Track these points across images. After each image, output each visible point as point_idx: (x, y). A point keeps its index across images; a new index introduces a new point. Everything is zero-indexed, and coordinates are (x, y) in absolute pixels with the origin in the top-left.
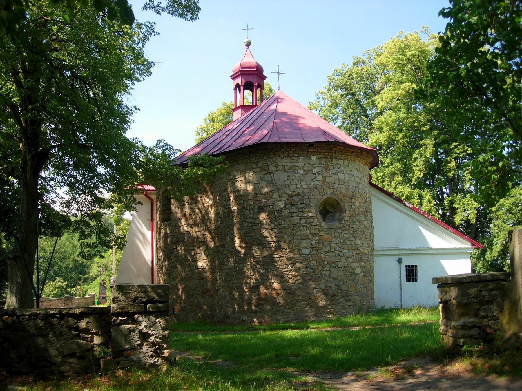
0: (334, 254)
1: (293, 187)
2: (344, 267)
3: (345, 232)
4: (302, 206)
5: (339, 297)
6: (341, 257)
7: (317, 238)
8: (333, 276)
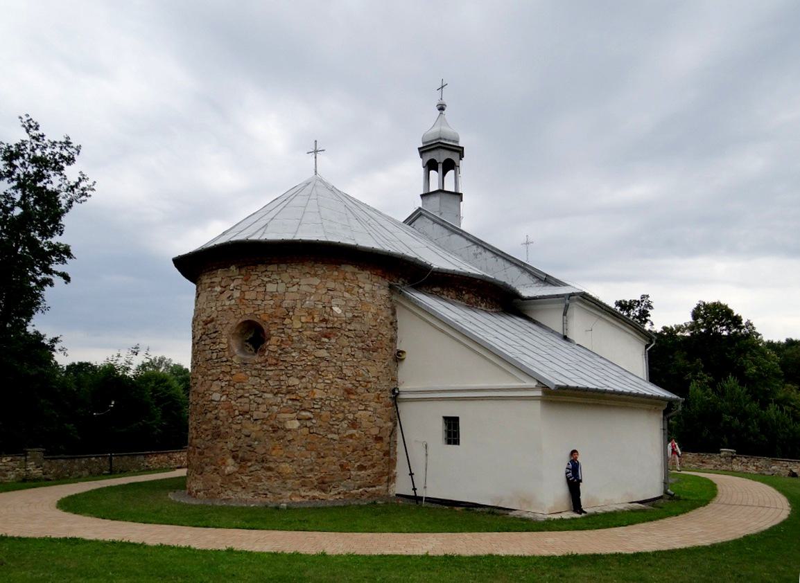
2: (263, 419)
3: (270, 368)
4: (214, 335)
5: (253, 463)
6: (258, 404)
7: (228, 378)
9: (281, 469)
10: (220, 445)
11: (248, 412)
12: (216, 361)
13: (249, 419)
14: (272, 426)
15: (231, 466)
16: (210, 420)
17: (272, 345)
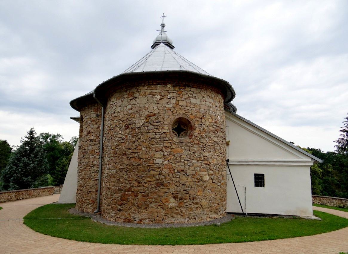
0: (183, 164)
2: (192, 175)
3: (195, 146)
4: (157, 124)
5: (187, 200)
6: (190, 166)
7: (169, 150)
9: (202, 203)
10: (163, 190)
11: (183, 171)
12: (160, 139)
13: (184, 175)
14: (197, 179)
15: (173, 203)
16: (154, 176)
17: (196, 132)
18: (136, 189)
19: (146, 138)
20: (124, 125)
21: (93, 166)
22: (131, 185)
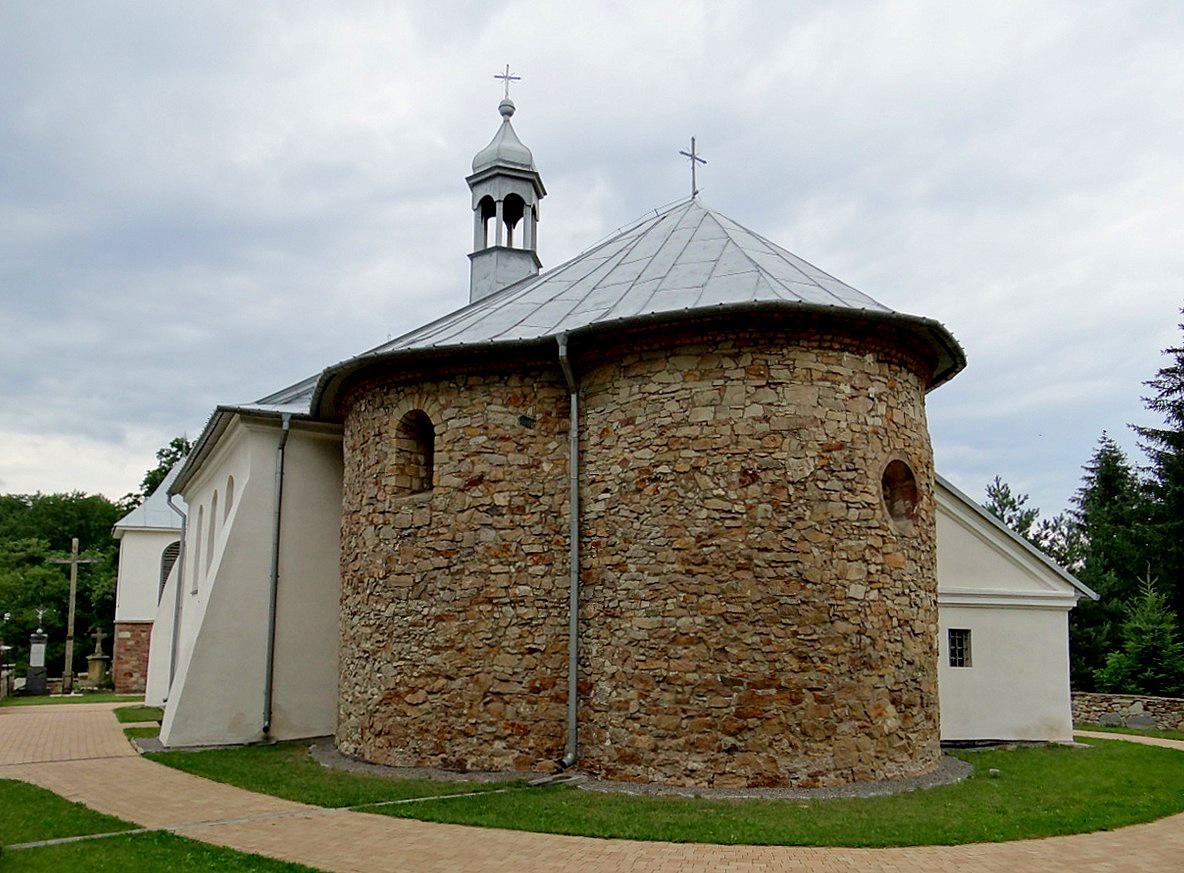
1: (831, 427)
4: (850, 475)
7: (880, 559)
8: (908, 656)
10: (869, 682)
12: (858, 524)
13: (909, 632)
16: (845, 637)
18: (796, 678)
19: (821, 517)
20: (739, 469)
21: (511, 602)
22: (778, 665)
